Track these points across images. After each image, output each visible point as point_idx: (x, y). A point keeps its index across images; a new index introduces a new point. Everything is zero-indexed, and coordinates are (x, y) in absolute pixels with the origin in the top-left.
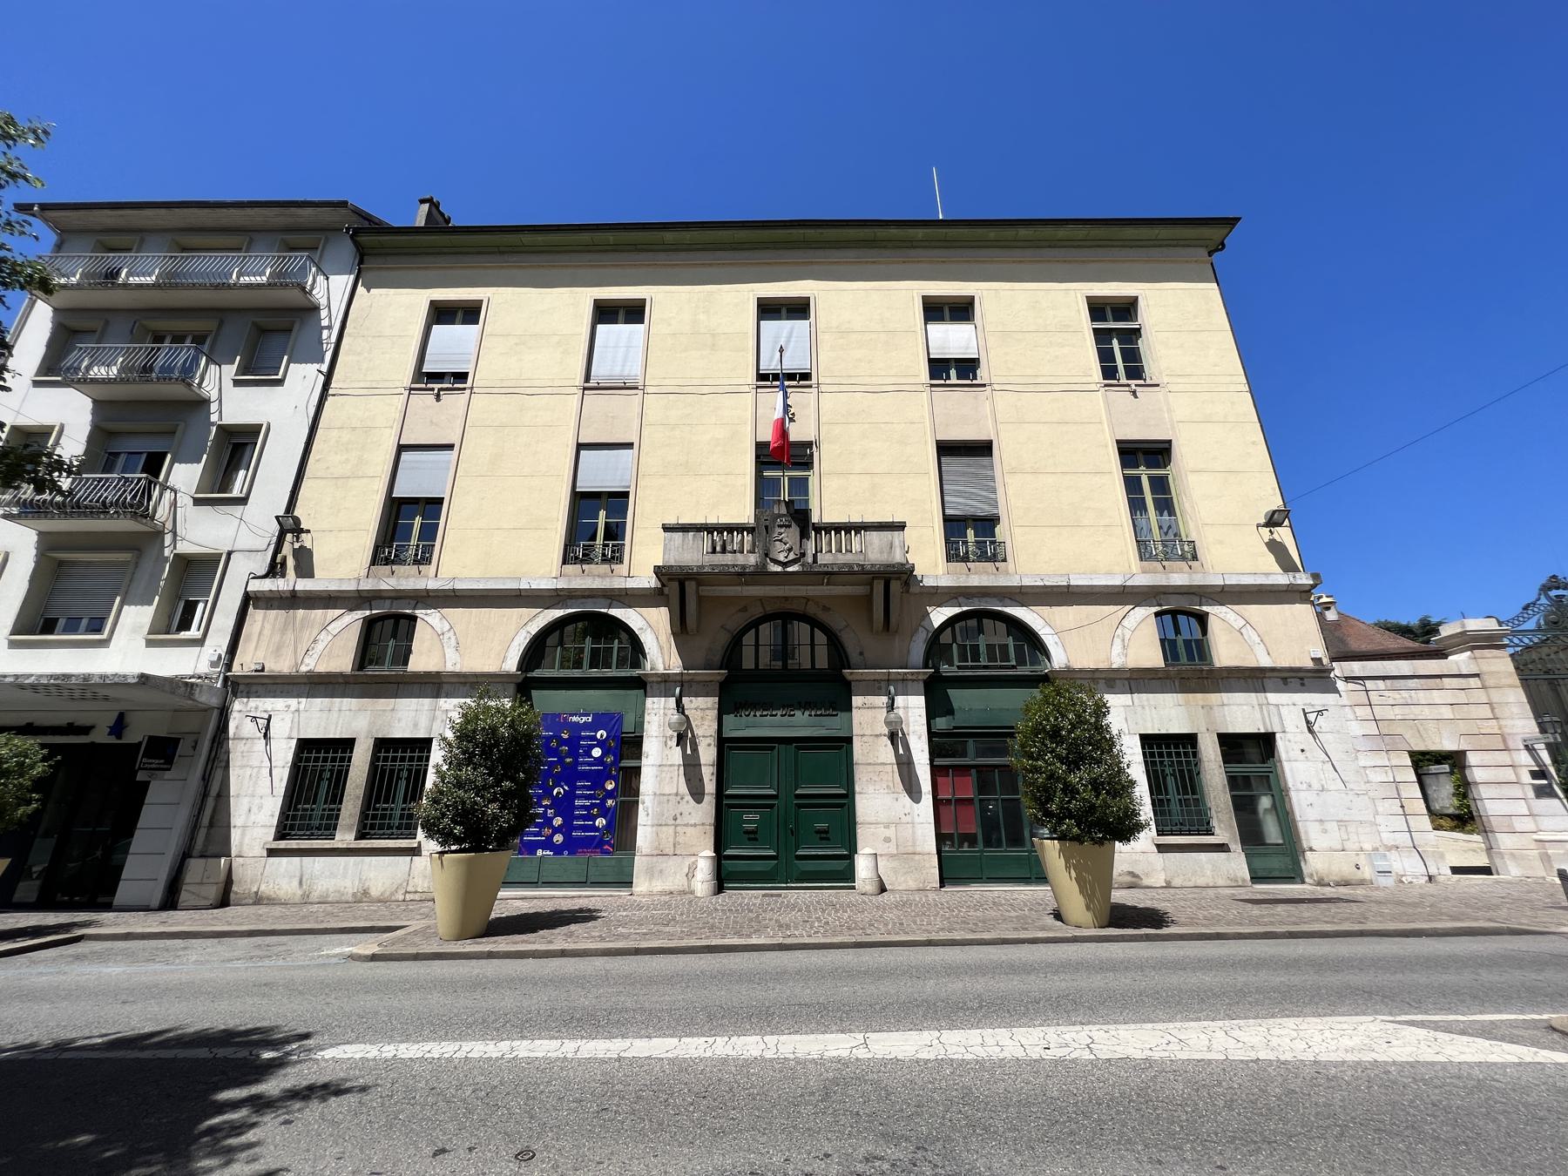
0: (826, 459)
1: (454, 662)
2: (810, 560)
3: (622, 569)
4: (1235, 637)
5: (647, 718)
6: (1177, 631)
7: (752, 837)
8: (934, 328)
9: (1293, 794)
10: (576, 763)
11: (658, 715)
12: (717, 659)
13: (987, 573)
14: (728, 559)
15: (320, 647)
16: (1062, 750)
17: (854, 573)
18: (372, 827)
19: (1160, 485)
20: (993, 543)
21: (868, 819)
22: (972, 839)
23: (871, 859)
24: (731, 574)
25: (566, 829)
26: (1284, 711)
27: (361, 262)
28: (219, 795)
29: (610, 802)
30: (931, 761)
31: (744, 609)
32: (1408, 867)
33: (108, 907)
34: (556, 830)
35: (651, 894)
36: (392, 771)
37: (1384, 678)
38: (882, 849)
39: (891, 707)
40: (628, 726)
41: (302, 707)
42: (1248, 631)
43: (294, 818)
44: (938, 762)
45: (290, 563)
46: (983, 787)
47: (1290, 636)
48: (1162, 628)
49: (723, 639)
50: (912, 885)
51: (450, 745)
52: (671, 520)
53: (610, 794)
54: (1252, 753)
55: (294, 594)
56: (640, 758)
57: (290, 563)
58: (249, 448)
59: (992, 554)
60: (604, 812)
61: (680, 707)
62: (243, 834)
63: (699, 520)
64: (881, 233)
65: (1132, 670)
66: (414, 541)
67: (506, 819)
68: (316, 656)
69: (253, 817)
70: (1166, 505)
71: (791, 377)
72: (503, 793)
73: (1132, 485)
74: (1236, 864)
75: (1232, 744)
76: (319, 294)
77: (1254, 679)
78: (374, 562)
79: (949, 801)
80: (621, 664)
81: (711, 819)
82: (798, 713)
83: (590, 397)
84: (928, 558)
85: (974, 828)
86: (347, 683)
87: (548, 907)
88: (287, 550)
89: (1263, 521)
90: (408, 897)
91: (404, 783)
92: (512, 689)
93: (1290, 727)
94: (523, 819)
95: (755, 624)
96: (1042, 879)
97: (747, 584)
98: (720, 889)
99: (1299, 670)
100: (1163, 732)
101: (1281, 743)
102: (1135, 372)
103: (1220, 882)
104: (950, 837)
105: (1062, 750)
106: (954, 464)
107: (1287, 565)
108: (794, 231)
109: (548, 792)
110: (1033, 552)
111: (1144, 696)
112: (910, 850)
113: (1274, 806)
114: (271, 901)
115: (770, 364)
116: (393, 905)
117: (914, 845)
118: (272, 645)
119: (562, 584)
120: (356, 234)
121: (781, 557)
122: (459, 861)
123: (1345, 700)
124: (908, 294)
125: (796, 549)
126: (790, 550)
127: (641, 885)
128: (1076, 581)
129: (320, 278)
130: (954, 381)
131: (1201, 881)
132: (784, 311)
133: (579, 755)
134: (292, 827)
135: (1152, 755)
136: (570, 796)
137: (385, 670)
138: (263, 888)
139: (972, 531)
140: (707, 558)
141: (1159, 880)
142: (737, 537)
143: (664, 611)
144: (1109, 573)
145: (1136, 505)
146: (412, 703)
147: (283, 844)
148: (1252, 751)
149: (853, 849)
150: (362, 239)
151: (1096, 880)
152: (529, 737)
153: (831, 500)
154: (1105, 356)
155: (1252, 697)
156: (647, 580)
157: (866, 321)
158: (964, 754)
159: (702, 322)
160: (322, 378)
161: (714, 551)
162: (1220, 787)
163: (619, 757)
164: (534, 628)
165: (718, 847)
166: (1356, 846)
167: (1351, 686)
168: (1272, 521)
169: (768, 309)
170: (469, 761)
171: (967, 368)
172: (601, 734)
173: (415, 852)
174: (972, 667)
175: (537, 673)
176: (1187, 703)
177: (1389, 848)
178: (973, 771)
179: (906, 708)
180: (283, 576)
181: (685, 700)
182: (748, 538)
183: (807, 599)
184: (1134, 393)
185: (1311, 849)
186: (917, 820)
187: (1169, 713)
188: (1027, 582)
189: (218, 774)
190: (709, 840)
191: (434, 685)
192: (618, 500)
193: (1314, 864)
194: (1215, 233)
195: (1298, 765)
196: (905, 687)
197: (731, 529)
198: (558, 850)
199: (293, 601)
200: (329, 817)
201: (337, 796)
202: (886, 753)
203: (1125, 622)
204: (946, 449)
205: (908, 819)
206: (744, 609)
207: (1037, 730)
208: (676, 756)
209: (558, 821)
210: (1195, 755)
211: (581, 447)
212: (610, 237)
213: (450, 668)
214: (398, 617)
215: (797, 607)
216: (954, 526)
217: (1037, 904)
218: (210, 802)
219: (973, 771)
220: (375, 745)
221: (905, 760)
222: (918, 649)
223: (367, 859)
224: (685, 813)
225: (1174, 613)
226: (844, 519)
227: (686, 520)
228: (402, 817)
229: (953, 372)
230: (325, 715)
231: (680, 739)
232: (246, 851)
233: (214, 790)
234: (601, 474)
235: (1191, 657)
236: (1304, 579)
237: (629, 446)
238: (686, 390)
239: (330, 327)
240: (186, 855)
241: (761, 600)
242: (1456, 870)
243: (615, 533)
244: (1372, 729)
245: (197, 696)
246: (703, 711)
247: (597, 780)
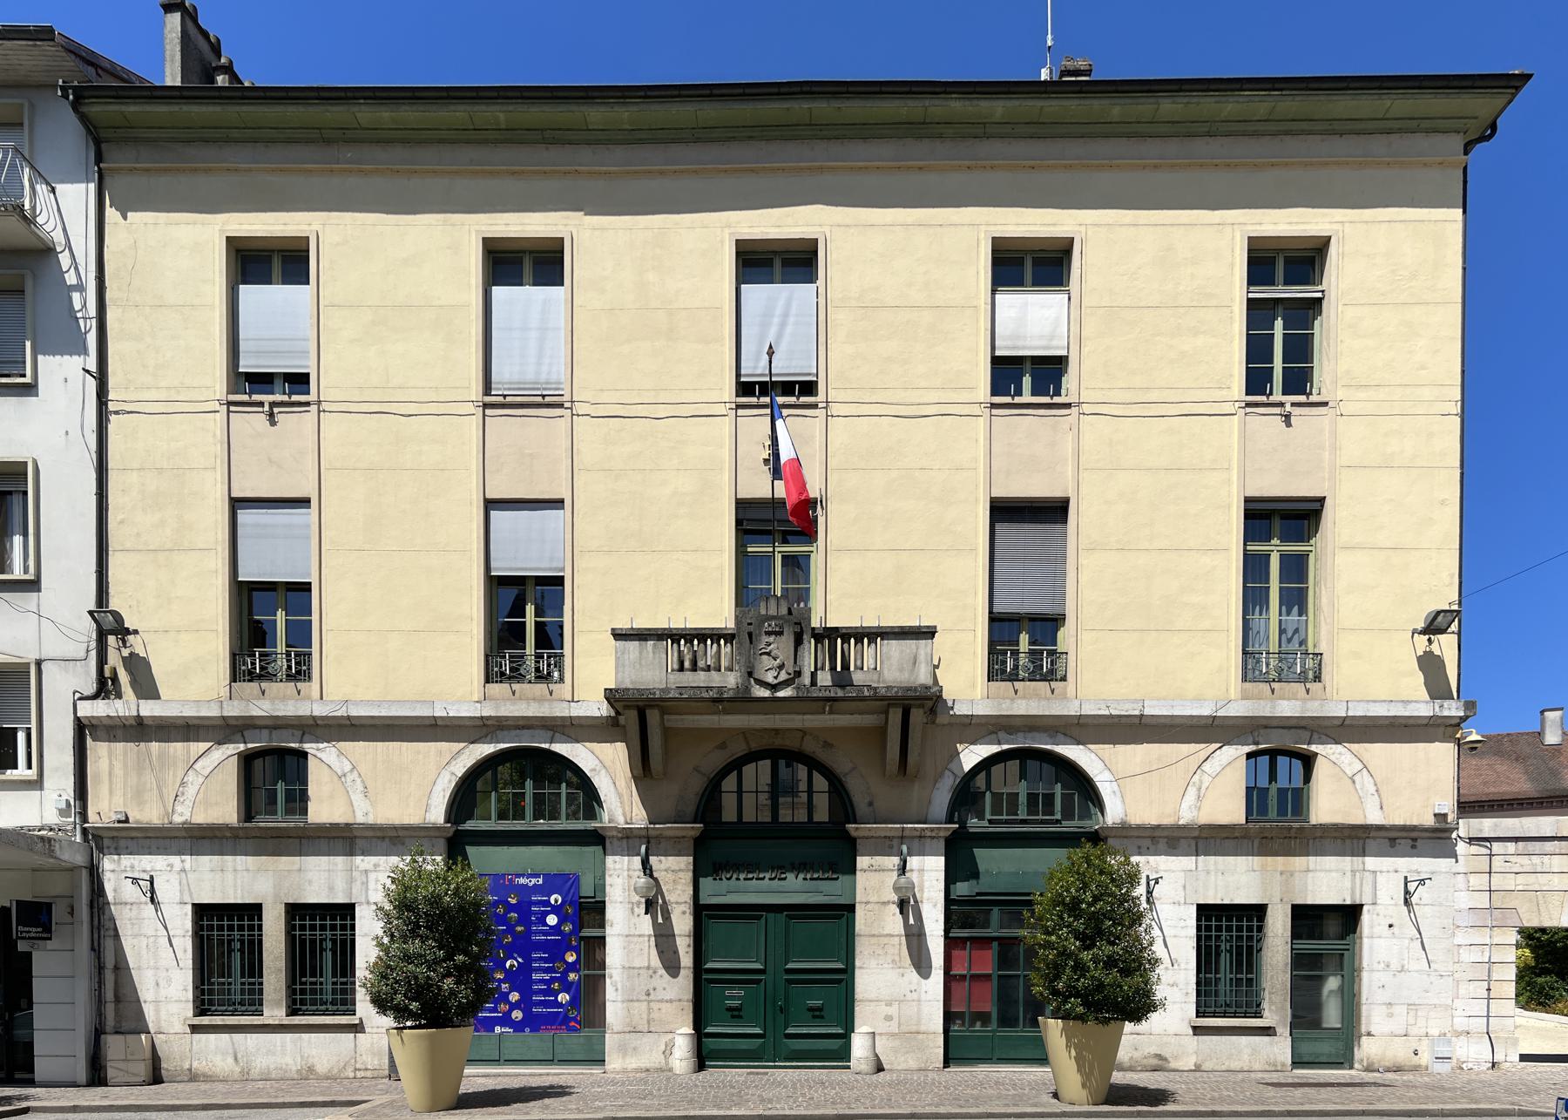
1: (364, 812)
2: (807, 680)
3: (564, 690)
4: (1342, 786)
6: (1273, 777)
7: (736, 1014)
8: (1009, 301)
9: (1365, 975)
10: (528, 932)
11: (621, 878)
12: (690, 809)
13: (1039, 697)
14: (700, 679)
15: (191, 791)
16: (1080, 925)
17: (864, 699)
18: (303, 1002)
19: (1296, 568)
20: (1052, 653)
21: (867, 996)
22: (984, 1018)
23: (868, 1039)
24: (703, 700)
25: (523, 1004)
26: (1381, 879)
27: (99, 159)
28: (116, 968)
29: (572, 976)
30: (947, 931)
31: (723, 746)
32: (1474, 1053)
33: (31, 1083)
34: (514, 1006)
35: (625, 1071)
36: (313, 942)
37: (1516, 839)
38: (881, 1027)
39: (903, 869)
40: (586, 889)
41: (187, 866)
42: (1365, 781)
43: (211, 992)
44: (955, 933)
45: (123, 677)
46: (1005, 960)
47: (1420, 781)
48: (1252, 773)
49: (697, 785)
50: (913, 1064)
51: (387, 914)
52: (623, 624)
53: (573, 967)
54: (1329, 930)
55: (140, 721)
56: (602, 925)
57: (123, 677)
58: (16, 500)
59: (1047, 668)
60: (566, 987)
61: (646, 868)
62: (157, 1011)
63: (660, 623)
64: (938, 108)
65: (1202, 828)
66: (281, 647)
67: (465, 994)
68: (189, 803)
69: (163, 993)
70: (1296, 599)
71: (787, 388)
72: (456, 967)
73: (1254, 567)
74: (1280, 1049)
75: (1307, 918)
76: (46, 221)
77: (1355, 839)
78: (234, 679)
79: (964, 977)
80: (574, 815)
81: (688, 994)
82: (790, 876)
83: (500, 424)
84: (964, 677)
85: (990, 1007)
86: (236, 837)
87: (515, 1084)
88: (114, 659)
89: (1421, 625)
90: (359, 1074)
91: (329, 954)
92: (442, 844)
93: (1383, 897)
94: (482, 994)
95: (736, 765)
96: (1043, 1060)
97: (726, 712)
98: (701, 1066)
99: (1413, 828)
100: (1226, 902)
101: (1366, 918)
102: (1298, 381)
103: (1257, 1066)
104: (961, 1015)
105: (1080, 925)
106: (1015, 534)
107: (1437, 687)
109: (500, 965)
110: (1103, 668)
111: (1213, 858)
112: (914, 1028)
113: (1341, 989)
114: (209, 1078)
115: (755, 368)
116: (345, 1082)
117: (919, 1022)
118: (125, 786)
119: (488, 711)
120: (80, 97)
122: (420, 1036)
123: (1461, 867)
124: (970, 231)
126: (781, 667)
127: (614, 1062)
128: (1152, 709)
129: (41, 189)
130: (1027, 398)
131: (1235, 1065)
132: (777, 263)
133: (531, 923)
134: (211, 1002)
135: (1208, 928)
136: (526, 969)
137: (279, 821)
138: (195, 1064)
139: (1025, 636)
140: (671, 677)
141: (1188, 1063)
142: (711, 649)
143: (621, 747)
144: (1199, 699)
145: (1253, 598)
146: (322, 862)
147: (205, 1020)
148: (1332, 925)
149: (849, 1027)
150: (95, 109)
151: (1096, 1061)
152: (476, 905)
153: (839, 597)
154: (1257, 349)
155: (1346, 862)
156: (597, 708)
157: (905, 270)
158: (986, 925)
159: (652, 273)
160: (92, 384)
161: (681, 669)
162: (1281, 965)
163: (579, 926)
164: (461, 767)
165: (698, 1024)
166: (1423, 1031)
167: (1474, 849)
168: (1433, 627)
169: (756, 262)
170: (414, 932)
171: (1047, 372)
172: (555, 898)
173: (358, 1028)
174: (1007, 822)
175: (470, 825)
176: (1263, 869)
177: (1458, 1034)
178: (995, 944)
179: (921, 871)
180: (119, 696)
181: (653, 859)
182: (726, 650)
183: (804, 732)
184: (1287, 419)
185: (1369, 1034)
186: (923, 997)
187: (1237, 879)
188: (1089, 710)
189: (109, 944)
190: (689, 1017)
191: (345, 839)
192: (551, 586)
193: (1367, 1049)
194: (1478, 105)
195: (1380, 945)
196: (920, 845)
197: (702, 636)
198: (518, 1027)
199: (139, 730)
200: (251, 992)
201: (254, 967)
202: (893, 923)
203: (1206, 767)
204: (1005, 511)
206: (723, 746)
207: (1057, 901)
208: (645, 924)
209: (514, 997)
210: (1260, 929)
211: (491, 504)
212: (498, 114)
213: (360, 819)
214: (282, 753)
215: (791, 743)
216: (1002, 627)
217: (1035, 1086)
218: (109, 977)
219: (995, 944)
220: (287, 912)
221: (915, 931)
222: (941, 798)
223: (305, 1036)
224: (659, 989)
225: (1273, 754)
226: (854, 623)
227: (642, 623)
228: (334, 992)
229: (1027, 381)
230: (218, 875)
231: (650, 906)
232: (165, 1026)
233: (110, 962)
234: (526, 547)
235: (1282, 811)
236: (1453, 709)
237: (557, 503)
238: (633, 411)
239: (80, 288)
240: (98, 1033)
241: (744, 733)
242: (1524, 1058)
243: (550, 638)
244: (1483, 900)
245: (58, 853)
246: (675, 872)
247: (555, 951)
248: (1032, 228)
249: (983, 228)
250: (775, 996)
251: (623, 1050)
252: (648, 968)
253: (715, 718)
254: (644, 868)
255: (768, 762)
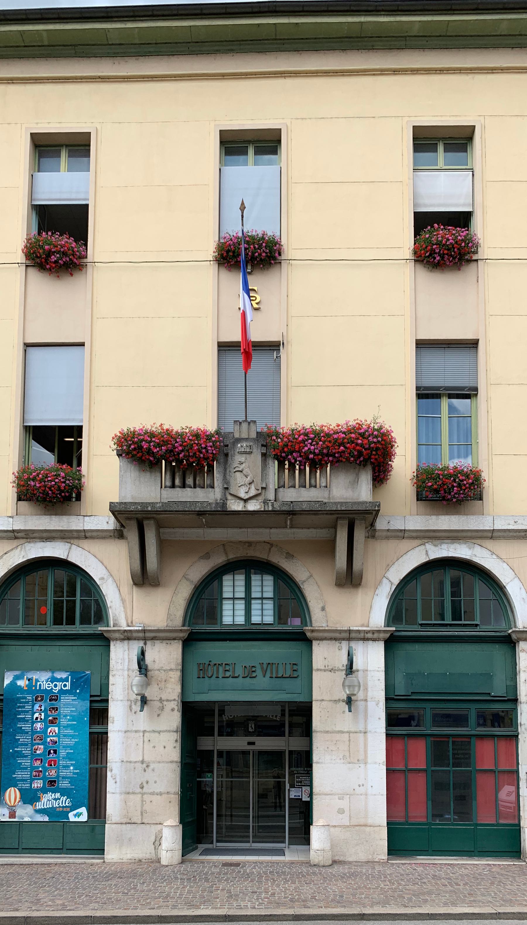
0: (295, 364)
2: (271, 496)
5: (112, 680)
108: (125, 74)
112: (362, 821)
121: (243, 495)
125: (258, 479)
127: (113, 853)
205: (362, 790)
211: (27, 345)
224: (151, 782)
248: (443, 119)
249: (406, 119)
250: (243, 777)
251: (120, 841)
252: (142, 762)
253: (200, 531)
254: (140, 667)
255: (244, 597)
